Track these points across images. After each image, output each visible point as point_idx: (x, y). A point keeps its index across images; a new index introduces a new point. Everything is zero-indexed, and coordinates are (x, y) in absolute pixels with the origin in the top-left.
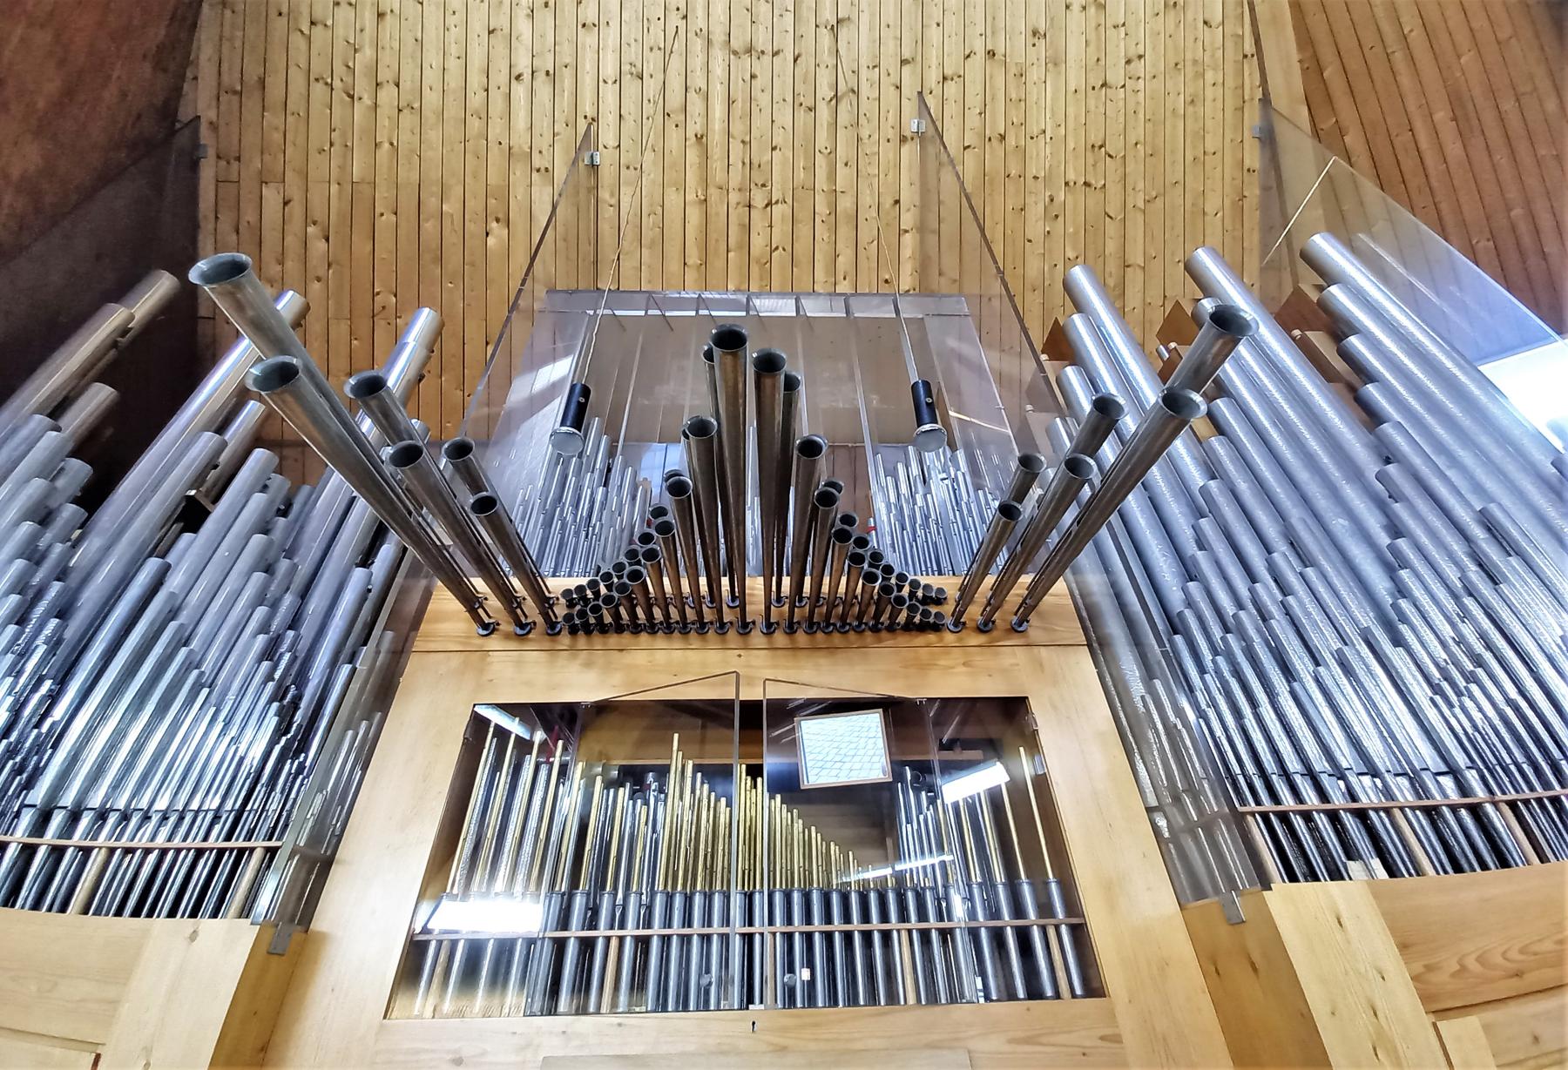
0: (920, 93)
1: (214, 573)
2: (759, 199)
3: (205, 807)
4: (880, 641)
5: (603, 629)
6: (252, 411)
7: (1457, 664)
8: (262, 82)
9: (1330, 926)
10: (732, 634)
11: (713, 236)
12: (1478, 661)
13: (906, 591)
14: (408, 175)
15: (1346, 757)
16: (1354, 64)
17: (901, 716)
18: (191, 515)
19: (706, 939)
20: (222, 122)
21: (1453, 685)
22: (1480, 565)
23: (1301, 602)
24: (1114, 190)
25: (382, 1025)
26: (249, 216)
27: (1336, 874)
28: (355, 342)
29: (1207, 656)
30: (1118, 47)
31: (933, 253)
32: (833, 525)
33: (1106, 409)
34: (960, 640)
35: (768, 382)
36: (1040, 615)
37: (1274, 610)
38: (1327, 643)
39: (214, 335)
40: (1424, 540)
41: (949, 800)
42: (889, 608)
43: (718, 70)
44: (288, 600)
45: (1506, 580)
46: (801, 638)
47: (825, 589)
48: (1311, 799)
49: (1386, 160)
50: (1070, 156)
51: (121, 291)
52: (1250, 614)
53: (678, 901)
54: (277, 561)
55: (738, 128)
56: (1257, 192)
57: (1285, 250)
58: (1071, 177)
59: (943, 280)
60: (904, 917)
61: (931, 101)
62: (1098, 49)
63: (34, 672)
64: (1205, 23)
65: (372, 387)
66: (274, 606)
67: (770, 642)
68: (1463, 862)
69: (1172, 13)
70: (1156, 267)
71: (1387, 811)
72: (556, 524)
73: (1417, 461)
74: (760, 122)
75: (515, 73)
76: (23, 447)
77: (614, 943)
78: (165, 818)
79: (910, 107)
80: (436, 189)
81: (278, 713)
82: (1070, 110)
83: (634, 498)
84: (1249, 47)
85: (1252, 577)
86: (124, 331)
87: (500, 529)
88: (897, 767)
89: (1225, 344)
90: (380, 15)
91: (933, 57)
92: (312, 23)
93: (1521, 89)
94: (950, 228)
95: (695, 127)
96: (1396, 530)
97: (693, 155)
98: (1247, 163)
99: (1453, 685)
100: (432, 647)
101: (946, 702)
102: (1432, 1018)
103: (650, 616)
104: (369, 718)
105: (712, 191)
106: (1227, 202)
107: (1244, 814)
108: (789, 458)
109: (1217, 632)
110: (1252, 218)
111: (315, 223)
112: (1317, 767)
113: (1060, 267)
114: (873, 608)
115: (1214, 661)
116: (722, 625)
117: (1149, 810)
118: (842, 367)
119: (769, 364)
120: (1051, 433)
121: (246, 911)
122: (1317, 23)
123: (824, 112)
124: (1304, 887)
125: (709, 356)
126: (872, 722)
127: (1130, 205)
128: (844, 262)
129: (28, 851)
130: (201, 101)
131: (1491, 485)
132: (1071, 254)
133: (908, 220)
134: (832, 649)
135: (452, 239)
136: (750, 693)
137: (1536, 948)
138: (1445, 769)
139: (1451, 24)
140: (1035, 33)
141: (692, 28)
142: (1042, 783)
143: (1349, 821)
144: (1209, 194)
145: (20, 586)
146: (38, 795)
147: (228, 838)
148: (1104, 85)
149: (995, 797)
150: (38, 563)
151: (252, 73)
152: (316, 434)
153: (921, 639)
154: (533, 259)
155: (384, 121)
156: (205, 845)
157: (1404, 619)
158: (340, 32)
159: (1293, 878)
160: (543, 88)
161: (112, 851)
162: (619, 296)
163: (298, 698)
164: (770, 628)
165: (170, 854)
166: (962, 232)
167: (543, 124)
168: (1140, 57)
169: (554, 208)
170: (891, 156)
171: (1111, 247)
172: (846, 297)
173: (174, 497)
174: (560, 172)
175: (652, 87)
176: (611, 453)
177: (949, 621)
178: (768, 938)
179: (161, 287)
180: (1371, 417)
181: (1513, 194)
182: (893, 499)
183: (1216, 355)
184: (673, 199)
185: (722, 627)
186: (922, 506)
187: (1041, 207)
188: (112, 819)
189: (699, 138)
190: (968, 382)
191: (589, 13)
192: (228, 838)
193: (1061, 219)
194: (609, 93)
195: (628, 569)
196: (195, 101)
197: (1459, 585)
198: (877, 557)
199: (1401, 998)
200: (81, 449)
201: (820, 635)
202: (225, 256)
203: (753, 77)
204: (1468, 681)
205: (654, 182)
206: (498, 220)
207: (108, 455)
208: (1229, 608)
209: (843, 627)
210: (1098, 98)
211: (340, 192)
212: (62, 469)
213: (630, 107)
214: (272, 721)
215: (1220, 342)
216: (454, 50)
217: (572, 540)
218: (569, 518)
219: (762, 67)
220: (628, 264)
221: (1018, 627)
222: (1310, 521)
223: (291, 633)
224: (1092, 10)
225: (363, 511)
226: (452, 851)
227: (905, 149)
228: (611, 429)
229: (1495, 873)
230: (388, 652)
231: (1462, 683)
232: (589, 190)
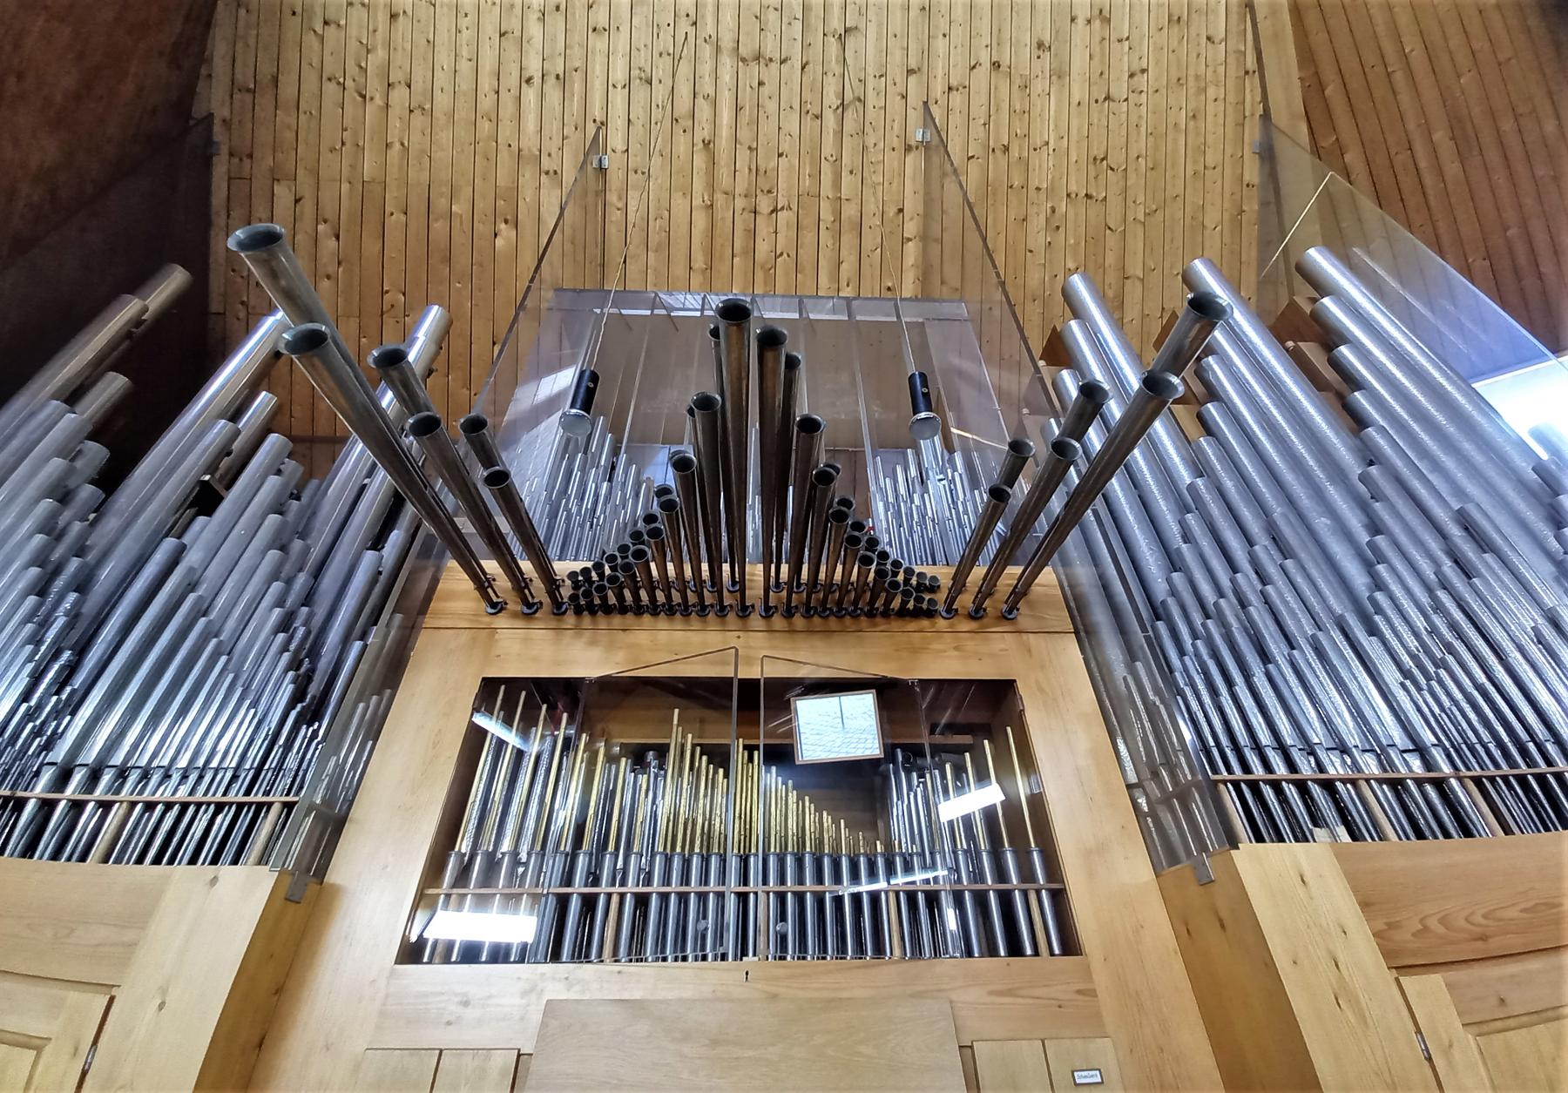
0: (926, 103)
1: (231, 556)
2: (765, 205)
3: (225, 765)
4: (875, 625)
5: (608, 610)
6: (264, 401)
7: (1428, 652)
8: (275, 81)
9: (1295, 886)
11: (718, 241)
13: (900, 578)
14: (418, 175)
15: (1317, 735)
16: (1356, 84)
17: (893, 697)
18: (204, 499)
19: (702, 897)
20: (235, 120)
22: (1456, 562)
23: (1279, 591)
24: (1115, 204)
25: (392, 972)
27: (1301, 837)
30: (1123, 61)
31: (936, 262)
32: (830, 506)
33: (1092, 395)
34: (951, 626)
35: (769, 355)
36: (1030, 605)
38: (1301, 627)
40: (1403, 539)
41: (944, 819)
42: (883, 595)
43: (727, 77)
44: (302, 579)
45: (1479, 575)
46: (799, 621)
47: (822, 576)
48: (1281, 770)
49: (1385, 178)
50: (1072, 168)
51: (136, 283)
52: (1229, 601)
53: (677, 863)
54: (291, 540)
55: (745, 135)
57: (1282, 266)
58: (1073, 188)
59: (945, 289)
61: (936, 112)
62: (1102, 62)
63: (54, 642)
64: (1209, 38)
65: (393, 359)
66: (289, 582)
67: (768, 625)
69: (1176, 29)
71: (1354, 782)
72: (562, 515)
73: (1399, 463)
74: (767, 128)
75: (526, 75)
76: (39, 432)
77: (615, 899)
78: (185, 777)
79: (915, 117)
80: (446, 190)
81: (294, 681)
82: (1074, 123)
83: (637, 495)
84: (1251, 62)
85: (1234, 568)
86: (137, 322)
87: (510, 502)
88: (890, 750)
89: (1202, 327)
90: (394, 16)
91: (939, 67)
92: (326, 23)
93: (1520, 110)
95: (702, 133)
96: (1375, 528)
97: (700, 161)
98: (1247, 178)
100: (442, 623)
101: (941, 683)
103: (653, 598)
104: (379, 693)
105: (719, 197)
106: (1226, 216)
107: (1216, 782)
108: (790, 437)
109: (1197, 618)
110: (1251, 232)
113: (1060, 278)
114: (868, 595)
115: (1193, 645)
116: (723, 608)
117: (1129, 787)
118: (845, 378)
120: (1044, 430)
122: (1319, 39)
123: (830, 119)
124: (1270, 847)
125: (715, 333)
126: (863, 705)
128: (847, 269)
129: (47, 806)
130: (215, 99)
131: (1472, 489)
132: (1071, 265)
133: (911, 229)
134: (828, 632)
135: (460, 239)
137: (1499, 914)
139: (1451, 44)
140: (1040, 45)
141: (702, 35)
142: (1037, 802)
143: (1316, 790)
144: (1208, 208)
145: (40, 559)
146: (60, 753)
147: (247, 793)
148: (1107, 98)
149: (989, 814)
150: (59, 537)
151: (266, 70)
152: (342, 401)
153: (913, 625)
154: (540, 260)
155: (395, 123)
156: (225, 799)
157: (1379, 610)
158: (353, 31)
159: (1259, 839)
160: (553, 93)
161: (133, 804)
162: (626, 297)
163: (312, 670)
164: (768, 612)
165: (191, 810)
166: (963, 237)
167: (553, 127)
168: (1143, 71)
169: (562, 209)
171: (1111, 259)
172: (848, 300)
174: (569, 176)
175: (660, 92)
176: (615, 451)
177: (941, 607)
178: (762, 897)
179: (174, 280)
180: (1357, 422)
181: (1510, 215)
182: (891, 499)
183: (1195, 338)
184: (680, 204)
185: (722, 611)
186: (920, 503)
188: (133, 777)
189: (706, 144)
190: (967, 394)
191: (600, 18)
192: (247, 793)
193: (1062, 229)
194: (618, 97)
195: (632, 548)
197: (1433, 576)
198: (873, 543)
199: (1363, 954)
200: (98, 432)
201: (816, 619)
202: (262, 226)
203: (761, 84)
204: (1437, 666)
206: (506, 222)
207: (126, 438)
209: (840, 613)
210: (1101, 112)
212: (80, 452)
213: (638, 112)
214: (287, 689)
215: (1198, 326)
216: (465, 52)
217: (576, 531)
218: (574, 510)
219: (771, 74)
220: (633, 268)
221: (1008, 615)
222: (1293, 518)
223: (305, 610)
224: (1097, 24)
225: (382, 480)
226: (447, 868)
227: (910, 158)
228: (616, 428)
230: (400, 627)
231: (1431, 669)
232: (597, 194)
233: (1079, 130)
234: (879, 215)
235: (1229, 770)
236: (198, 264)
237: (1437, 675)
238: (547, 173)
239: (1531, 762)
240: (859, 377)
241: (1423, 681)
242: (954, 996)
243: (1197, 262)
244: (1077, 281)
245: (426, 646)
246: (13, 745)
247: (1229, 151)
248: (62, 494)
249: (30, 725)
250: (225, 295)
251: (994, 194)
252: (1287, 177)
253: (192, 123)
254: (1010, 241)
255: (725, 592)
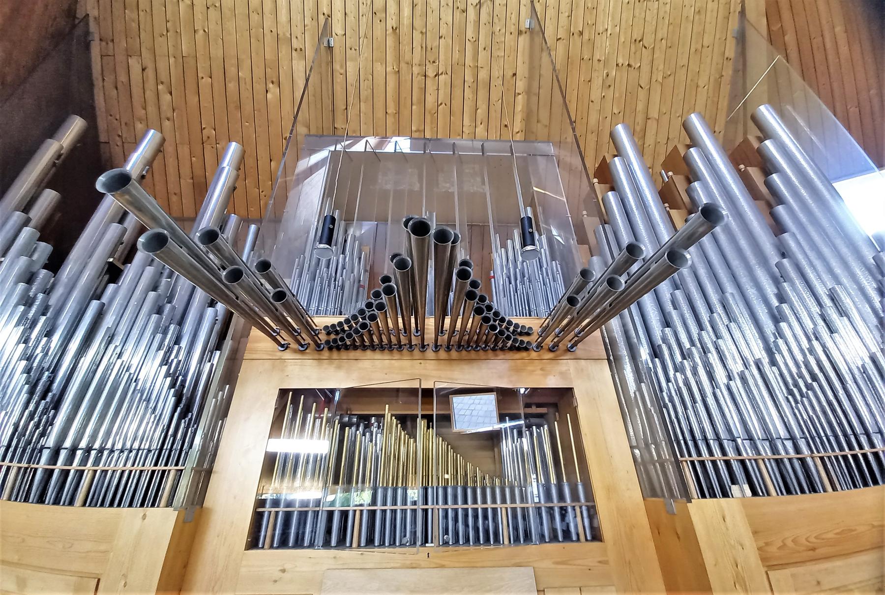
2: (431, 73)
4: (497, 356)
5: (347, 348)
10: (416, 352)
11: (403, 96)
12: (814, 378)
17: (505, 396)
18: (113, 273)
21: (800, 390)
23: (726, 344)
24: (646, 69)
26: (123, 78)
27: (725, 494)
28: (194, 159)
29: (671, 373)
31: (535, 108)
34: (539, 356)
37: (710, 346)
39: (110, 153)
46: (454, 354)
51: (52, 131)
55: (418, 23)
56: (730, 72)
57: (742, 113)
59: (539, 125)
60: (504, 501)
68: (792, 489)
70: (665, 119)
72: (318, 280)
77: (358, 513)
80: (235, 61)
81: (174, 395)
83: (360, 258)
85: (701, 328)
94: (545, 93)
95: (391, 22)
97: (390, 41)
99: (800, 390)
100: (254, 356)
102: (766, 569)
105: (403, 65)
107: (682, 461)
110: (726, 89)
111: (162, 83)
112: (722, 436)
115: (675, 375)
117: (632, 447)
119: (442, 236)
121: (169, 504)
124: (709, 501)
126: (492, 398)
127: (654, 80)
133: (521, 85)
135: (246, 94)
136: (427, 385)
137: (824, 536)
138: (789, 437)
155: (199, 16)
166: (553, 98)
167: (297, 18)
170: (512, 43)
171: (640, 107)
173: (101, 263)
174: (310, 52)
179: (75, 126)
180: (778, 228)
184: (379, 68)
186: (523, 282)
187: (601, 79)
189: (394, 30)
192: (156, 465)
193: (612, 88)
196: (85, 4)
199: (750, 556)
201: (464, 352)
205: (366, 59)
206: (273, 83)
207: (60, 235)
208: (687, 344)
211: (175, 62)
212: (36, 248)
214: (171, 400)
223: (176, 347)
227: (521, 39)
229: (809, 496)
233: (626, 21)
234: (501, 79)
235: (690, 455)
236: (89, 113)
237: (807, 393)
238: (296, 50)
239: (851, 448)
240: (486, 179)
241: (799, 398)
242: (536, 565)
243: (693, 116)
244: (620, 129)
245: (246, 370)
246: (24, 436)
247: (718, 37)
248: (29, 278)
249: (32, 422)
250: (108, 131)
251: (572, 64)
252: (751, 54)
253: (77, 21)
254: (580, 95)
255: (413, 337)
